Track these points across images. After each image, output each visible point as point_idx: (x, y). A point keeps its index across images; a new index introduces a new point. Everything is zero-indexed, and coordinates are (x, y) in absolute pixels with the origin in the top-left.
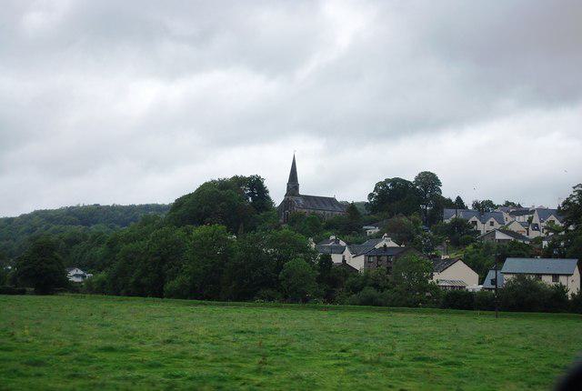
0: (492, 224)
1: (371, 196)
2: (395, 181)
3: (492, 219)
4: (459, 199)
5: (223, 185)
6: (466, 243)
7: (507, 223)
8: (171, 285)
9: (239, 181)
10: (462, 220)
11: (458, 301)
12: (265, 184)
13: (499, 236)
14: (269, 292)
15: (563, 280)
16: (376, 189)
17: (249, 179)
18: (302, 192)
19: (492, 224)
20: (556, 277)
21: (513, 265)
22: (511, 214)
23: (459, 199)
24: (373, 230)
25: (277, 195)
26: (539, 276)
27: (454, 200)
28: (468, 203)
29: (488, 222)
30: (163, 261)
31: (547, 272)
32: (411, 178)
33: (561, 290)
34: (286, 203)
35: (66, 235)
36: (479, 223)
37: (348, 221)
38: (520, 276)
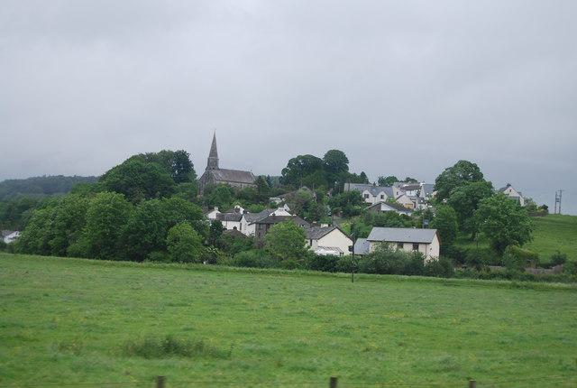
0: (382, 197)
1: (284, 171)
2: (305, 158)
3: (382, 193)
4: (363, 174)
5: (151, 158)
6: (356, 213)
7: (396, 197)
8: (72, 247)
9: (166, 156)
10: (353, 192)
11: (327, 265)
12: (191, 158)
13: (384, 208)
14: (160, 254)
15: (421, 249)
16: (290, 165)
17: (177, 153)
18: (221, 166)
19: (382, 197)
20: (416, 245)
21: (377, 233)
22: (402, 189)
23: (363, 174)
24: (278, 201)
25: (200, 168)
26: (401, 244)
27: (359, 174)
28: (373, 179)
29: (379, 196)
30: (69, 225)
31: (341, 281)
32: (321, 156)
33: (419, 258)
34: (207, 176)
35: (20, 202)
36: (371, 196)
37: (259, 193)
38: (385, 244)
